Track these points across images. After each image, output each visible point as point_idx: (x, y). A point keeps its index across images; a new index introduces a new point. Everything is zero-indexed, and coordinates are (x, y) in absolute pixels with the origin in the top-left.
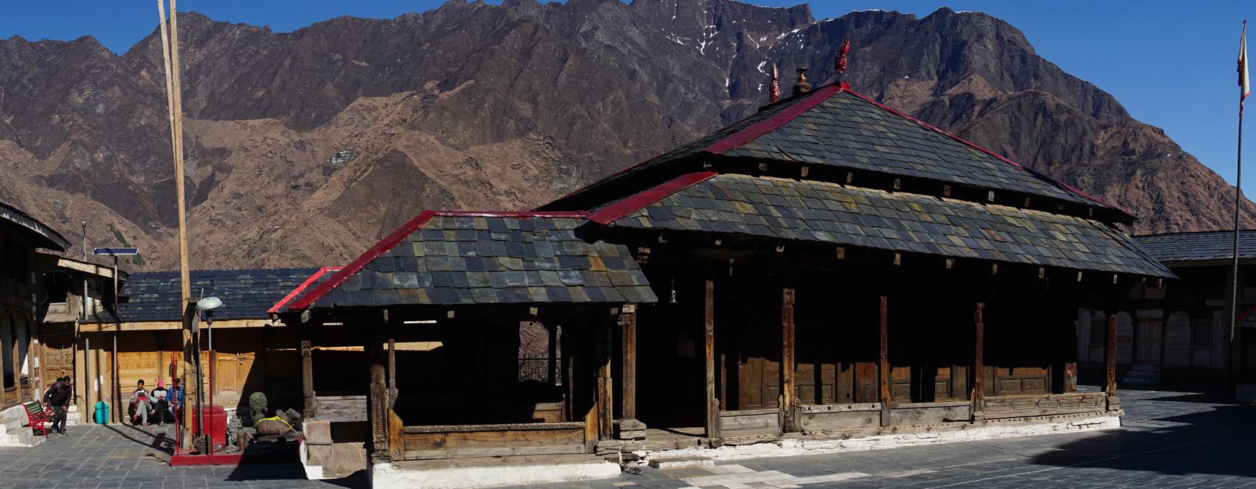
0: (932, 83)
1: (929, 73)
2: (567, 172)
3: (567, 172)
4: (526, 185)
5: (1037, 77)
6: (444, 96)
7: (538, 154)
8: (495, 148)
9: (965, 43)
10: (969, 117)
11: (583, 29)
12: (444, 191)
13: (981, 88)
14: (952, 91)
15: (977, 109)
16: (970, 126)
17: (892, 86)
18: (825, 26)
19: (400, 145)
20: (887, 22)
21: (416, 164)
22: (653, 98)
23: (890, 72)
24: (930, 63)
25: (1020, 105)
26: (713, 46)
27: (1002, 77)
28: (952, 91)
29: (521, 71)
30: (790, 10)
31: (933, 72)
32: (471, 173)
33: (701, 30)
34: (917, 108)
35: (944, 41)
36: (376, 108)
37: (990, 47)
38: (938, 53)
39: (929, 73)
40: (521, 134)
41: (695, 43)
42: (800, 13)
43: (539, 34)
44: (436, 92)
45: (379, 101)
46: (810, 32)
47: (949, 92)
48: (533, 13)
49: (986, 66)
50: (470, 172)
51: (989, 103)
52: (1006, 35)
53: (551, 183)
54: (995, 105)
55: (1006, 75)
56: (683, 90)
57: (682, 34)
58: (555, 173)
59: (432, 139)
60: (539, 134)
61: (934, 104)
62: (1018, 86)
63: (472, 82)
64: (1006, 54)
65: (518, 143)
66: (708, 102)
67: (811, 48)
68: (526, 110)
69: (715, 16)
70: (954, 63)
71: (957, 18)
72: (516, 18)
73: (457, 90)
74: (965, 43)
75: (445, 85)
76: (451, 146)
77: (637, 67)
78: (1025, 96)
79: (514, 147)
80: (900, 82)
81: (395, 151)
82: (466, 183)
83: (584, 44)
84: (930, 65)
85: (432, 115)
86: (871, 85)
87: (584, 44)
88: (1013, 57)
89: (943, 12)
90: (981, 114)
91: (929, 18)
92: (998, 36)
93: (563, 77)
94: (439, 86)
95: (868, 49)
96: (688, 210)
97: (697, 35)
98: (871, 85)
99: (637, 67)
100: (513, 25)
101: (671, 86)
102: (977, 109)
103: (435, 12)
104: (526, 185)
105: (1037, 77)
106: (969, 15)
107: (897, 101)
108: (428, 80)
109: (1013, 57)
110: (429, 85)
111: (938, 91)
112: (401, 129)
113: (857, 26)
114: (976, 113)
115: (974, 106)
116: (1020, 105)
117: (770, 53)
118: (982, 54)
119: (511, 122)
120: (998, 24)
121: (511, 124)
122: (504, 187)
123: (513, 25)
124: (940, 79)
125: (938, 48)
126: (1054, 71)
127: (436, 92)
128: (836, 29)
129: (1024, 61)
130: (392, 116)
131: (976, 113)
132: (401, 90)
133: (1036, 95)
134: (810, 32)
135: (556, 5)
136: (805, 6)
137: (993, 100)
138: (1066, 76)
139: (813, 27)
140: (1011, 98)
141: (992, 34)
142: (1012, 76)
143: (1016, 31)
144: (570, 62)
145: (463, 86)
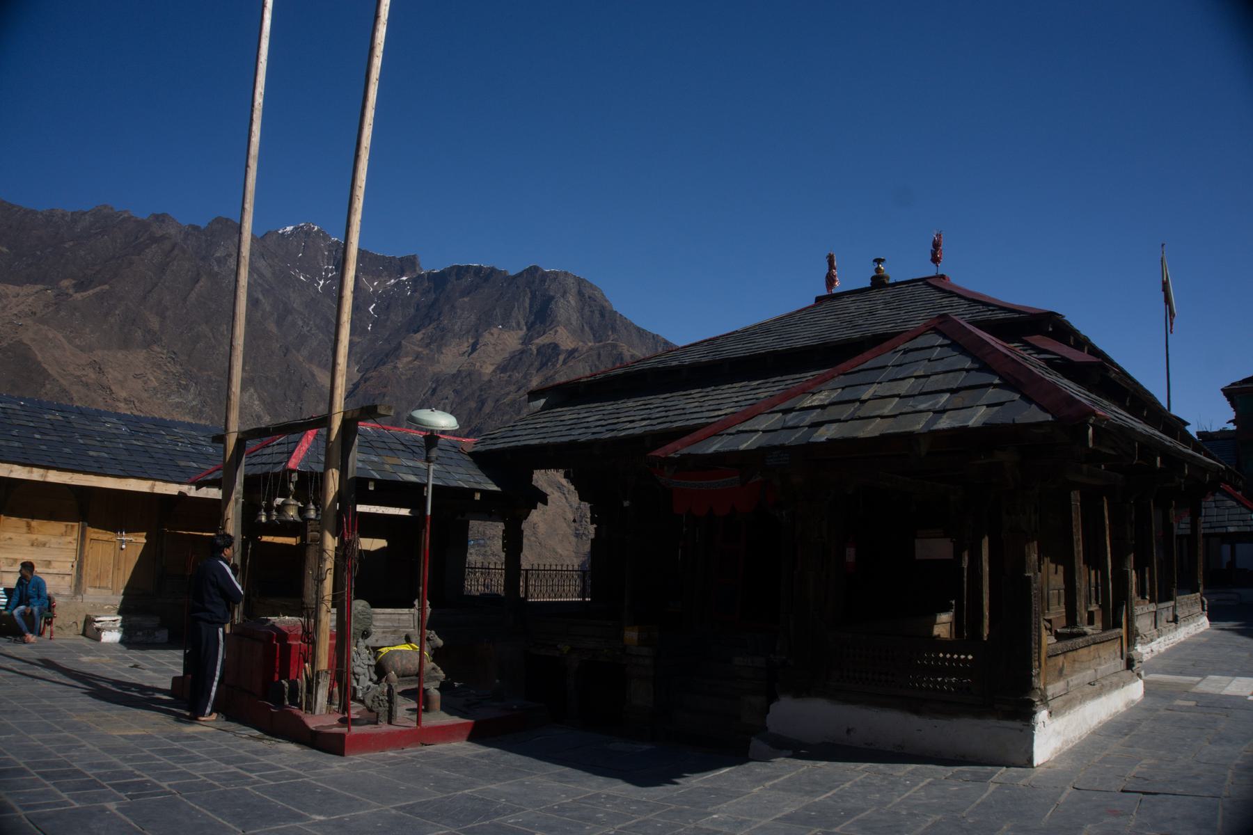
0: (522, 333)
1: (518, 324)
2: (186, 388)
3: (186, 388)
4: (145, 395)
5: (614, 329)
6: (78, 296)
7: (159, 367)
8: (119, 355)
9: (553, 298)
10: (554, 365)
11: (218, 254)
12: (64, 391)
13: (565, 339)
14: (540, 341)
15: (561, 358)
16: (556, 373)
17: (486, 334)
18: (432, 277)
19: (26, 337)
20: (485, 276)
21: (40, 358)
22: (272, 327)
23: (485, 321)
24: (520, 315)
25: (599, 355)
26: (331, 285)
27: (582, 330)
28: (540, 341)
29: (156, 285)
30: (401, 259)
31: (523, 323)
32: (93, 376)
33: (320, 270)
34: (507, 355)
35: (533, 297)
36: (7, 296)
37: (573, 302)
38: (527, 305)
39: (518, 324)
40: (147, 345)
41: (314, 280)
42: (408, 263)
43: (176, 252)
44: (71, 291)
45: (12, 289)
46: (418, 280)
47: (537, 341)
48: (173, 231)
49: (569, 319)
50: (93, 375)
51: (571, 353)
52: (587, 292)
53: (169, 396)
54: (576, 354)
55: (587, 329)
56: (300, 323)
57: (304, 270)
58: (174, 387)
59: (60, 336)
60: (163, 347)
61: (522, 352)
62: (597, 338)
63: (106, 287)
64: (587, 309)
65: (142, 354)
66: (321, 336)
67: (417, 295)
68: (155, 323)
69: (335, 258)
70: (542, 316)
71: (545, 275)
72: (159, 234)
73: (91, 292)
74: (553, 298)
75: (81, 286)
76: (77, 346)
77: (261, 297)
78: (604, 346)
79: (139, 357)
80: (494, 330)
81: (21, 342)
82: (87, 385)
83: (216, 268)
84: (520, 318)
85: (63, 313)
86: (468, 332)
87: (216, 268)
88: (592, 312)
89: (534, 269)
90: (565, 362)
91: (520, 275)
92: (580, 293)
93: (193, 296)
94: (75, 286)
95: (466, 299)
96: (426, 622)
97: (315, 274)
98: (468, 332)
99: (261, 297)
100: (154, 240)
101: (290, 318)
102: (561, 358)
103: (84, 213)
104: (145, 395)
105: (614, 329)
106: (556, 273)
107: (490, 348)
108: (65, 278)
109: (592, 312)
110: (65, 283)
111: (527, 340)
112: (30, 322)
113: (458, 277)
114: (560, 362)
115: (558, 355)
116: (599, 355)
117: (380, 297)
118: (566, 308)
119: (140, 332)
120: (580, 282)
121: (139, 334)
122: (124, 394)
123: (154, 240)
124: (528, 329)
125: (527, 301)
126: (628, 325)
127: (71, 291)
128: (439, 280)
129: (602, 316)
130: (22, 307)
131: (560, 362)
132: (35, 282)
133: (614, 346)
134: (418, 280)
135: (196, 228)
136: (414, 257)
137: (574, 351)
138: (638, 329)
139: (421, 276)
140: (591, 349)
141: (574, 291)
142: (591, 328)
143: (595, 288)
144: (201, 283)
145: (98, 289)
